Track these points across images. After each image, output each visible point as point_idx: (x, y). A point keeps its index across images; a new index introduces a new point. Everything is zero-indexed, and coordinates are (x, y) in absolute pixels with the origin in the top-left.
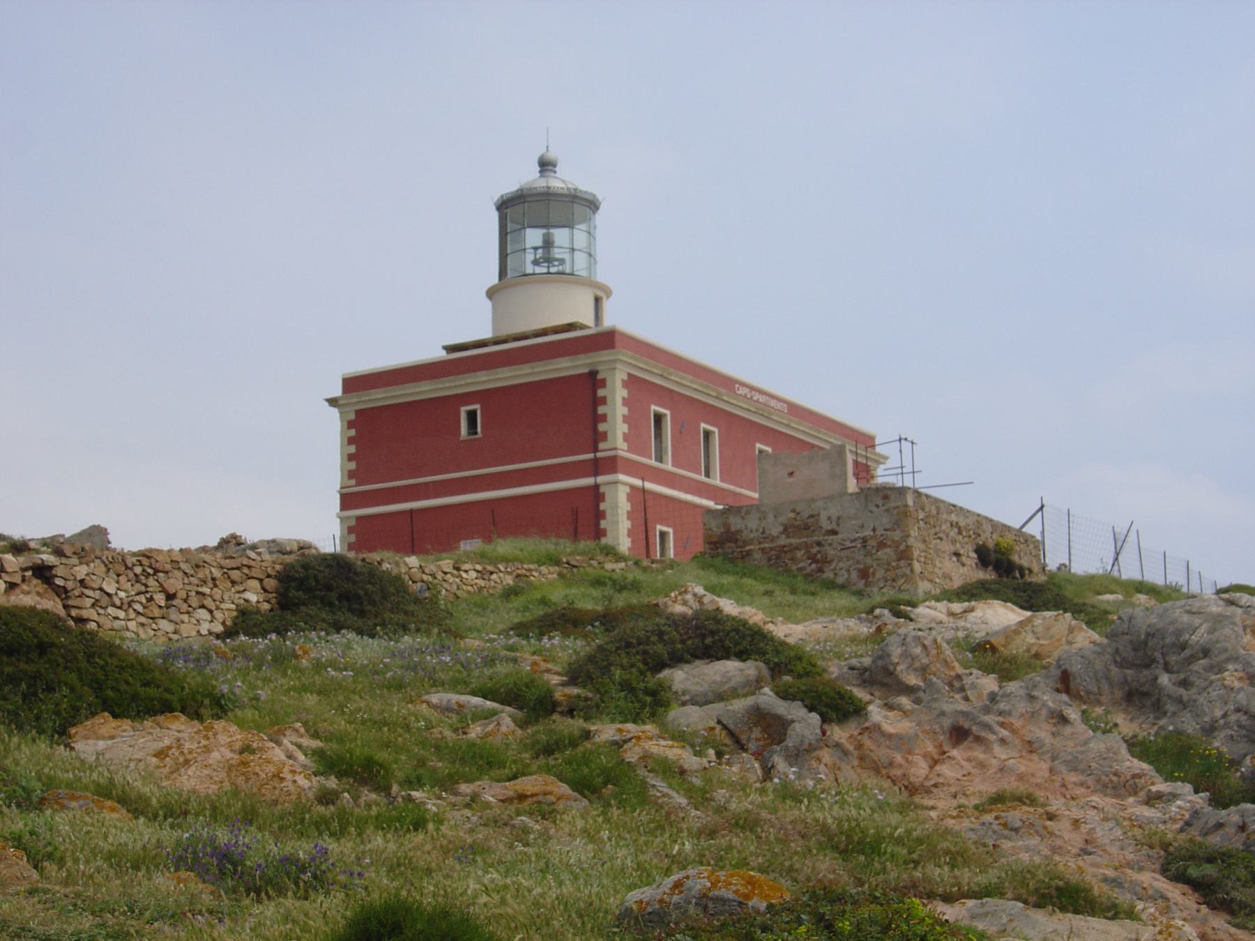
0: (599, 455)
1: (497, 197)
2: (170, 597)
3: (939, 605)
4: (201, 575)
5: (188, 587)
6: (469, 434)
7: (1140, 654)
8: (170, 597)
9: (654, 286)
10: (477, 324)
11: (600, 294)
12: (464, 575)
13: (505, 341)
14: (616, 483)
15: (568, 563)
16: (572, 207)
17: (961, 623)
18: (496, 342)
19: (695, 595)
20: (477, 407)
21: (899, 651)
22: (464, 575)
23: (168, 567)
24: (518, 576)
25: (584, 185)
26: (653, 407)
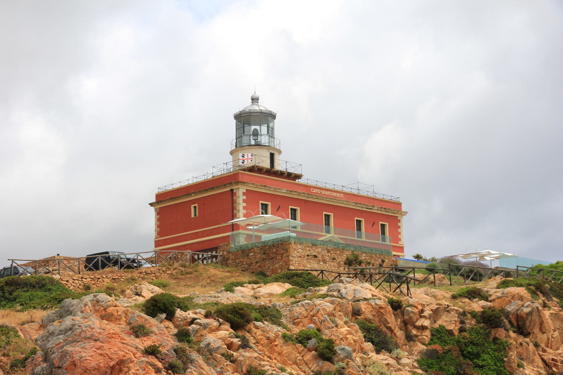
9: (297, 150)
11: (273, 152)
14: (239, 233)
16: (268, 117)
20: (196, 205)
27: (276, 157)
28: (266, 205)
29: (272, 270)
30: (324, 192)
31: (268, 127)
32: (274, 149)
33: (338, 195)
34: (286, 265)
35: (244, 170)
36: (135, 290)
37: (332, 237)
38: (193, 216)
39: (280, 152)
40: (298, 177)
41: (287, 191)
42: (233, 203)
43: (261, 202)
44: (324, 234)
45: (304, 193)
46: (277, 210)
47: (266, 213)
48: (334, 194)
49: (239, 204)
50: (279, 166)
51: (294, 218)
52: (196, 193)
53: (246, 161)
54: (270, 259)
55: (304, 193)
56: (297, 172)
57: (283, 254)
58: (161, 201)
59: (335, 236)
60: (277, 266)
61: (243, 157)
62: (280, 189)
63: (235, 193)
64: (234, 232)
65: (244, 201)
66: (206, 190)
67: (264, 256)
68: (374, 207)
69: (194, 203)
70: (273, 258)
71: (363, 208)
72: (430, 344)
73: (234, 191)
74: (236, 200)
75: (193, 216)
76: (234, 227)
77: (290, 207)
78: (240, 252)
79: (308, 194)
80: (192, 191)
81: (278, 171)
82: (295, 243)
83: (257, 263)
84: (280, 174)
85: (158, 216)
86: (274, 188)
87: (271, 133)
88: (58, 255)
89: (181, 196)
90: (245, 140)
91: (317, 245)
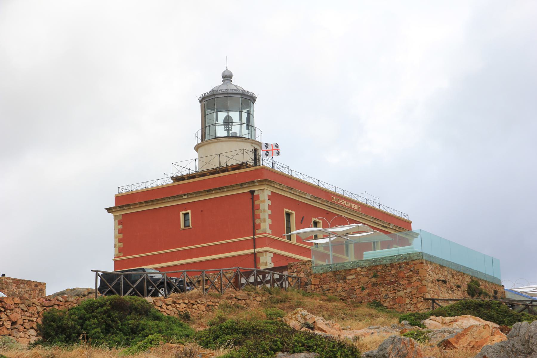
0: (256, 236)
1: (199, 95)
2: (14, 323)
3: (438, 318)
4: (31, 311)
5: (23, 318)
6: (185, 227)
7: (526, 346)
8: (14, 323)
10: (189, 163)
11: (257, 147)
12: (178, 306)
13: (205, 175)
15: (235, 298)
16: (247, 100)
17: (450, 328)
18: (202, 174)
19: (302, 315)
20: (189, 211)
21: (391, 346)
22: (178, 306)
23: (13, 307)
24: (208, 306)
25: (248, 88)
26: (285, 210)
29: (394, 299)
34: (419, 292)
36: (303, 321)
38: (182, 226)
42: (254, 208)
54: (387, 284)
57: (411, 276)
60: (402, 293)
63: (258, 196)
64: (256, 250)
66: (208, 191)
67: (374, 280)
68: (389, 224)
69: (186, 209)
70: (394, 283)
73: (256, 193)
75: (182, 226)
78: (330, 274)
83: (363, 289)
88: (3, 275)
89: (164, 199)
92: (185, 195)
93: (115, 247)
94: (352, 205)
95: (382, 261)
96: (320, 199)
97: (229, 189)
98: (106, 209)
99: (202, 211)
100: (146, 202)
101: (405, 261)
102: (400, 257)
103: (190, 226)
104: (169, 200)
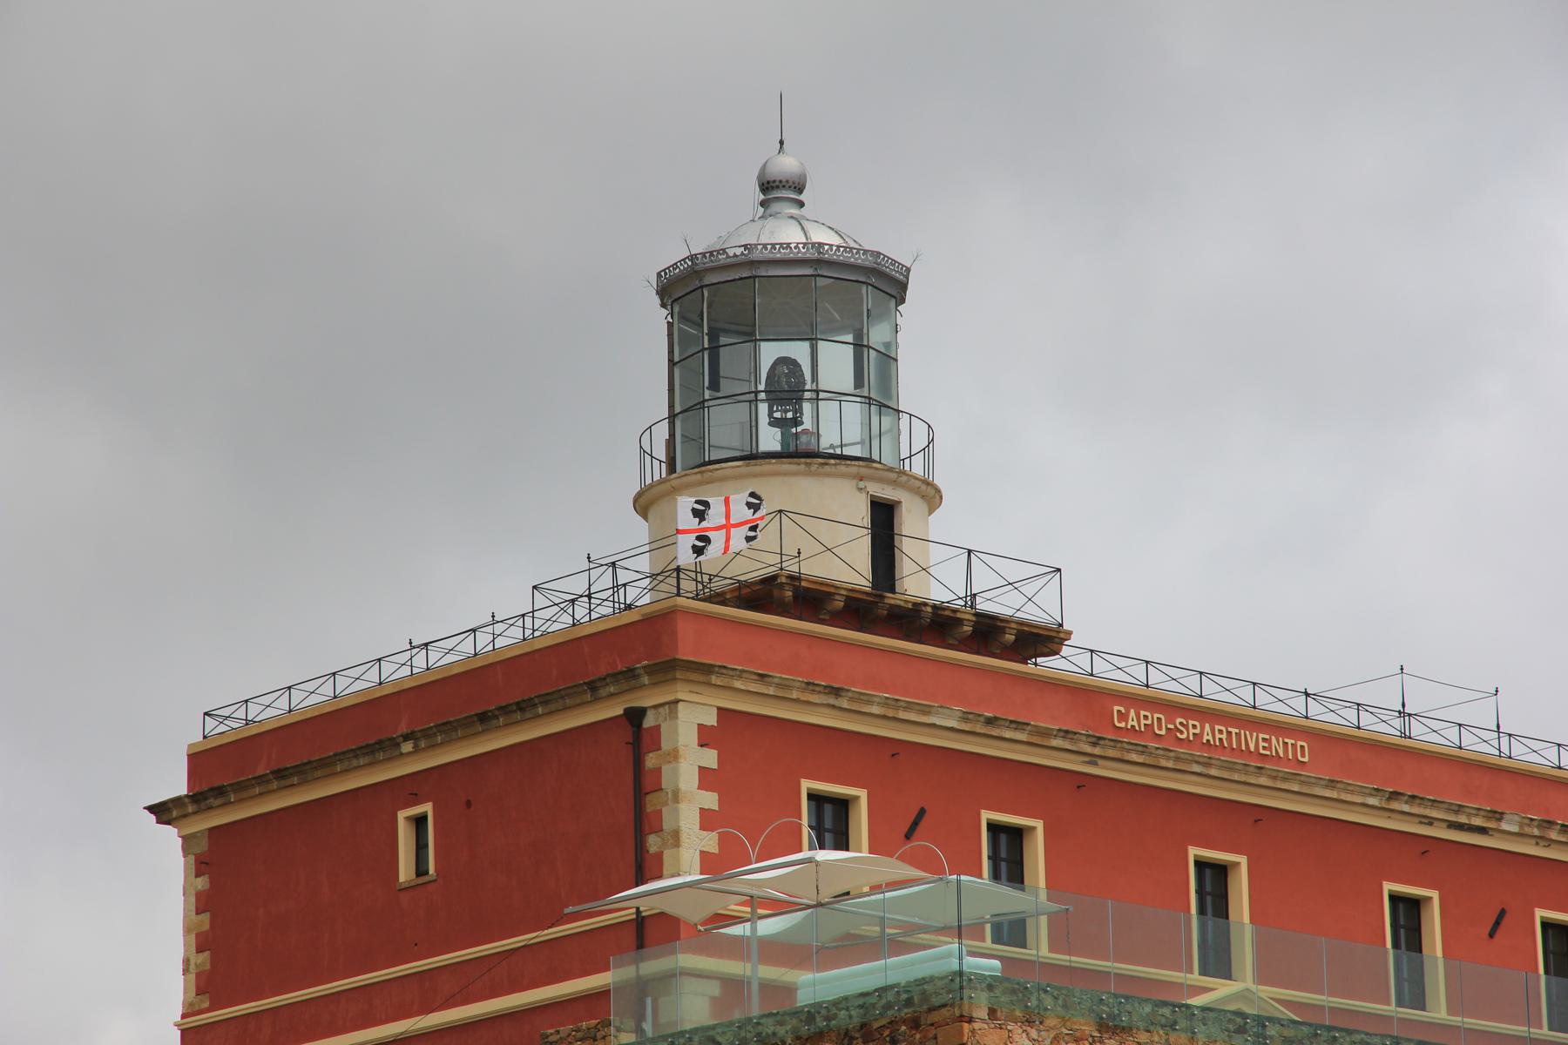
11: (887, 493)
20: (427, 808)
27: (909, 520)
28: (843, 806)
30: (1191, 728)
31: (859, 347)
32: (898, 476)
33: (1277, 745)
35: (719, 598)
37: (1244, 995)
38: (405, 871)
39: (931, 496)
40: (1043, 640)
41: (965, 717)
43: (806, 785)
44: (1195, 978)
45: (1066, 734)
46: (906, 832)
47: (842, 843)
48: (1254, 740)
49: (676, 797)
50: (933, 577)
51: (1009, 866)
52: (424, 737)
53: (717, 538)
55: (1066, 734)
56: (1037, 609)
58: (219, 791)
59: (1266, 991)
61: (699, 515)
62: (926, 710)
65: (707, 779)
66: (483, 718)
68: (1498, 816)
69: (416, 799)
71: (1430, 822)
72: (677, 701)
73: (649, 722)
74: (658, 772)
75: (405, 871)
76: (646, 932)
77: (986, 816)
79: (1096, 741)
80: (403, 728)
81: (918, 607)
82: (992, 1013)
84: (936, 624)
85: (202, 883)
86: (886, 703)
87: (876, 384)
89: (339, 757)
90: (723, 426)
91: (1127, 1030)
92: (406, 738)
93: (186, 971)
94: (1254, 740)
95: (835, 1017)
96: (1018, 725)
97: (553, 707)
98: (151, 809)
99: (469, 804)
100: (280, 774)
101: (907, 1012)
102: (890, 996)
103: (432, 870)
104: (355, 763)
